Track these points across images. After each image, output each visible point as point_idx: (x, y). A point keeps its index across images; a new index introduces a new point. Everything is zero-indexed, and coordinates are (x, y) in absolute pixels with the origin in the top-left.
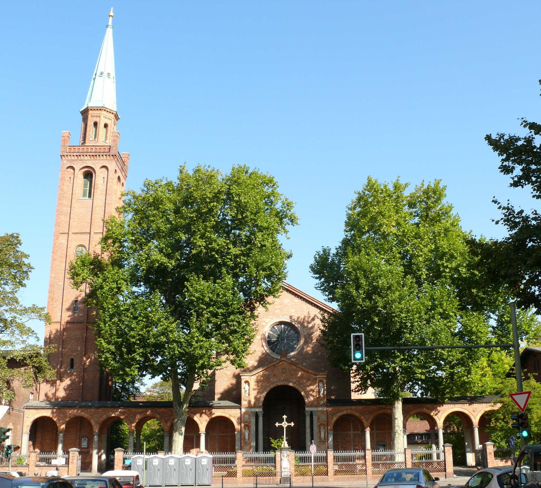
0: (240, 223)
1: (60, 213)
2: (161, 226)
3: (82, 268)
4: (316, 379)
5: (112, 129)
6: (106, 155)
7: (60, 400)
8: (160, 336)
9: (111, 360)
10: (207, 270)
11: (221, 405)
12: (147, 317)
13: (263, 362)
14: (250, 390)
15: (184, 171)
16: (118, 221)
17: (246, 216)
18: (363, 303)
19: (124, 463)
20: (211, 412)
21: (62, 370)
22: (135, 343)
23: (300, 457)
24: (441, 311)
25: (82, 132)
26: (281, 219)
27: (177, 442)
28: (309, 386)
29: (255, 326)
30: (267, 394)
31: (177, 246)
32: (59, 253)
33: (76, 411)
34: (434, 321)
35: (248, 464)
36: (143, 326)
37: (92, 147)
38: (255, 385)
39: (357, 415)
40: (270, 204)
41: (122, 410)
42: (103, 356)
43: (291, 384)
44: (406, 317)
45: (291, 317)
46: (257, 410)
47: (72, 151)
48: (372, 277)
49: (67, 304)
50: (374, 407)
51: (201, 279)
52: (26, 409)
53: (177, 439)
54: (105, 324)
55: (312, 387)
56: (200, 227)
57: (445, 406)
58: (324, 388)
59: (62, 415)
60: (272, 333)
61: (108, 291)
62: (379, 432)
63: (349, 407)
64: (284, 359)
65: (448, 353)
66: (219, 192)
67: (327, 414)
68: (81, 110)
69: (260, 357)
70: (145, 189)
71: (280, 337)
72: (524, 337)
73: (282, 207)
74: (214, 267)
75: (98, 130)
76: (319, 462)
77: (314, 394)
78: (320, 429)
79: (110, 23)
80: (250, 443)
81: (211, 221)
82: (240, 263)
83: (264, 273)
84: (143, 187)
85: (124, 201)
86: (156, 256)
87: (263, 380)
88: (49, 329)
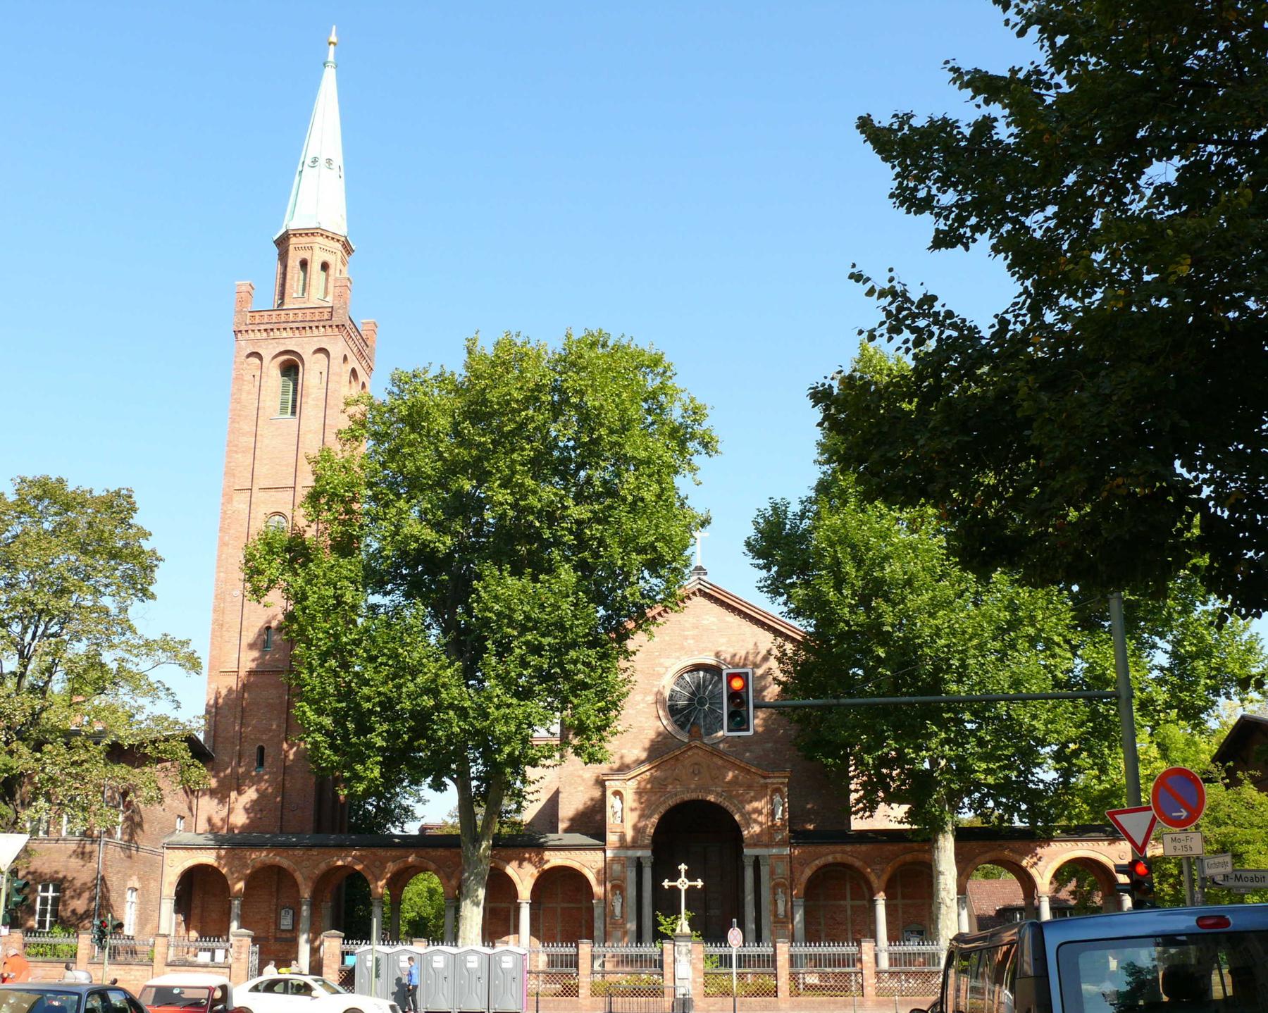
0: (591, 453)
1: (235, 449)
2: (423, 464)
3: (267, 557)
4: (765, 786)
5: (338, 272)
6: (324, 327)
7: (236, 831)
8: (421, 696)
9: (326, 748)
10: (522, 555)
11: (563, 842)
12: (395, 656)
13: (659, 751)
14: (625, 810)
15: (477, 349)
16: (338, 458)
17: (600, 437)
18: (850, 616)
19: (343, 963)
20: (542, 859)
21: (241, 770)
22: (371, 712)
23: (721, 956)
24: (1031, 631)
25: (279, 282)
26: (682, 443)
27: (468, 922)
28: (751, 802)
29: (629, 672)
30: (661, 820)
31: (464, 506)
32: (232, 531)
33: (264, 854)
34: (1016, 654)
35: (620, 969)
36: (387, 676)
37: (297, 311)
38: (634, 801)
39: (858, 864)
40: (658, 411)
41: (358, 853)
42: (309, 739)
43: (711, 798)
44: (948, 646)
45: (717, 655)
46: (639, 853)
47: (257, 321)
48: (871, 559)
49: (250, 635)
50: (890, 848)
51: (505, 574)
52: (167, 848)
53: (469, 915)
54: (311, 671)
55: (756, 804)
56: (501, 463)
57: (1054, 846)
58: (783, 805)
59: (236, 862)
60: (678, 689)
61: (316, 603)
62: (909, 902)
63: (838, 848)
64: (698, 743)
65: (1046, 726)
66: (539, 388)
67: (791, 862)
68: (275, 238)
69: (652, 741)
70: (396, 390)
71: (697, 696)
72: (1232, 691)
73: (683, 417)
74: (537, 548)
75: (308, 275)
76: (759, 967)
77: (762, 819)
78: (775, 894)
79: (331, 57)
80: (624, 924)
81: (523, 449)
82: (593, 538)
83: (639, 558)
84: (390, 387)
85: (351, 417)
86: (414, 527)
87: (652, 788)
88: (214, 686)
